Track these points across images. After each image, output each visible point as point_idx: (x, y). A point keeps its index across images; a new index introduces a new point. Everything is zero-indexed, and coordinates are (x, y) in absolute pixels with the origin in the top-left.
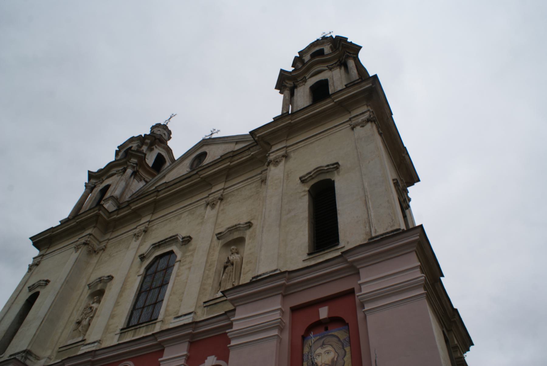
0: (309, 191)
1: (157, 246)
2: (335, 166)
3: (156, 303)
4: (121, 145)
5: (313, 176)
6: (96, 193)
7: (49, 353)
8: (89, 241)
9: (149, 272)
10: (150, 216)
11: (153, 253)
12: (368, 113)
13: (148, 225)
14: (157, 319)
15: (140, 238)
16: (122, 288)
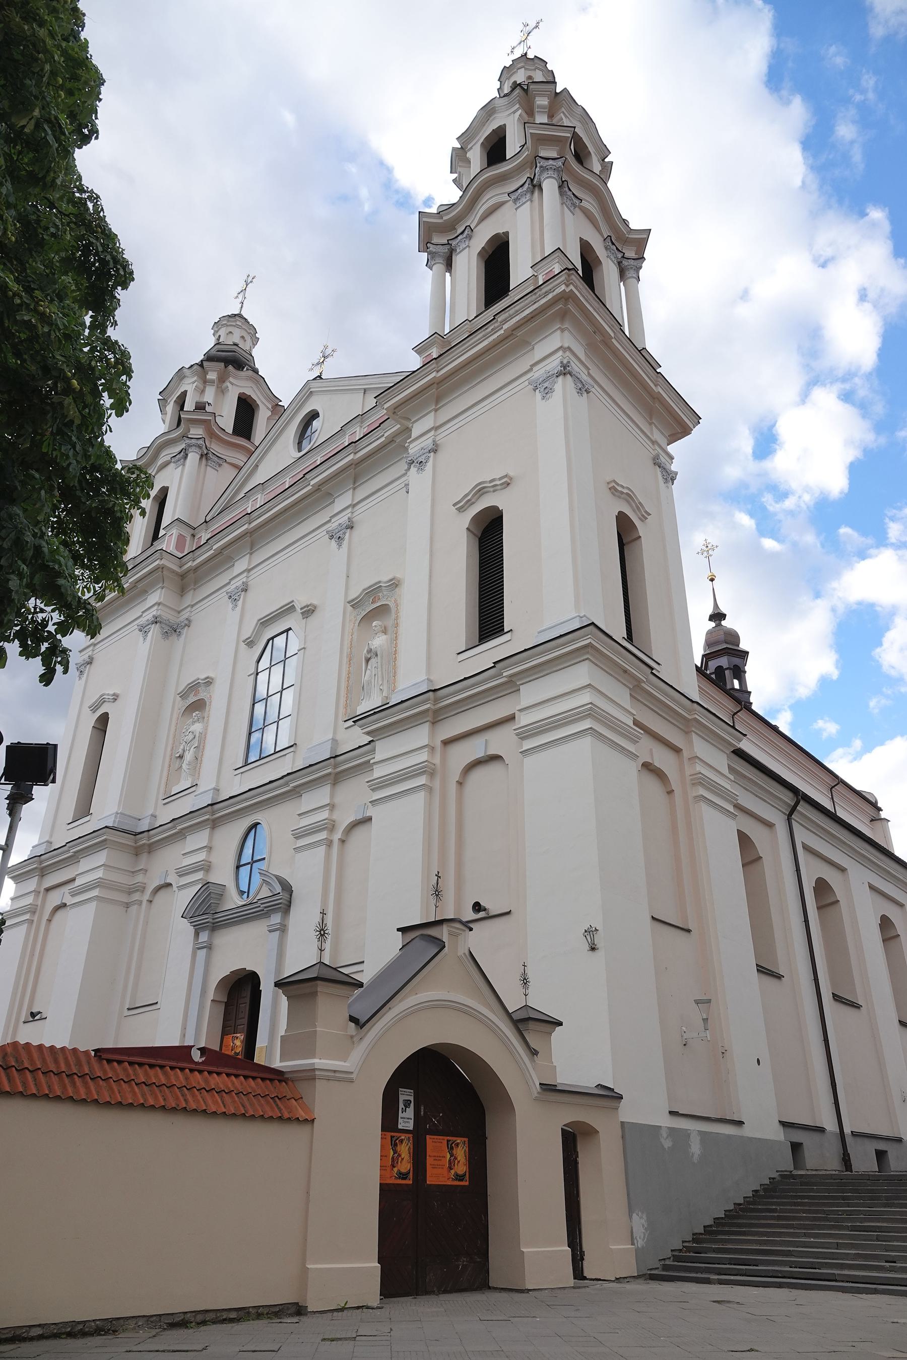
1: (265, 622)
12: (560, 353)
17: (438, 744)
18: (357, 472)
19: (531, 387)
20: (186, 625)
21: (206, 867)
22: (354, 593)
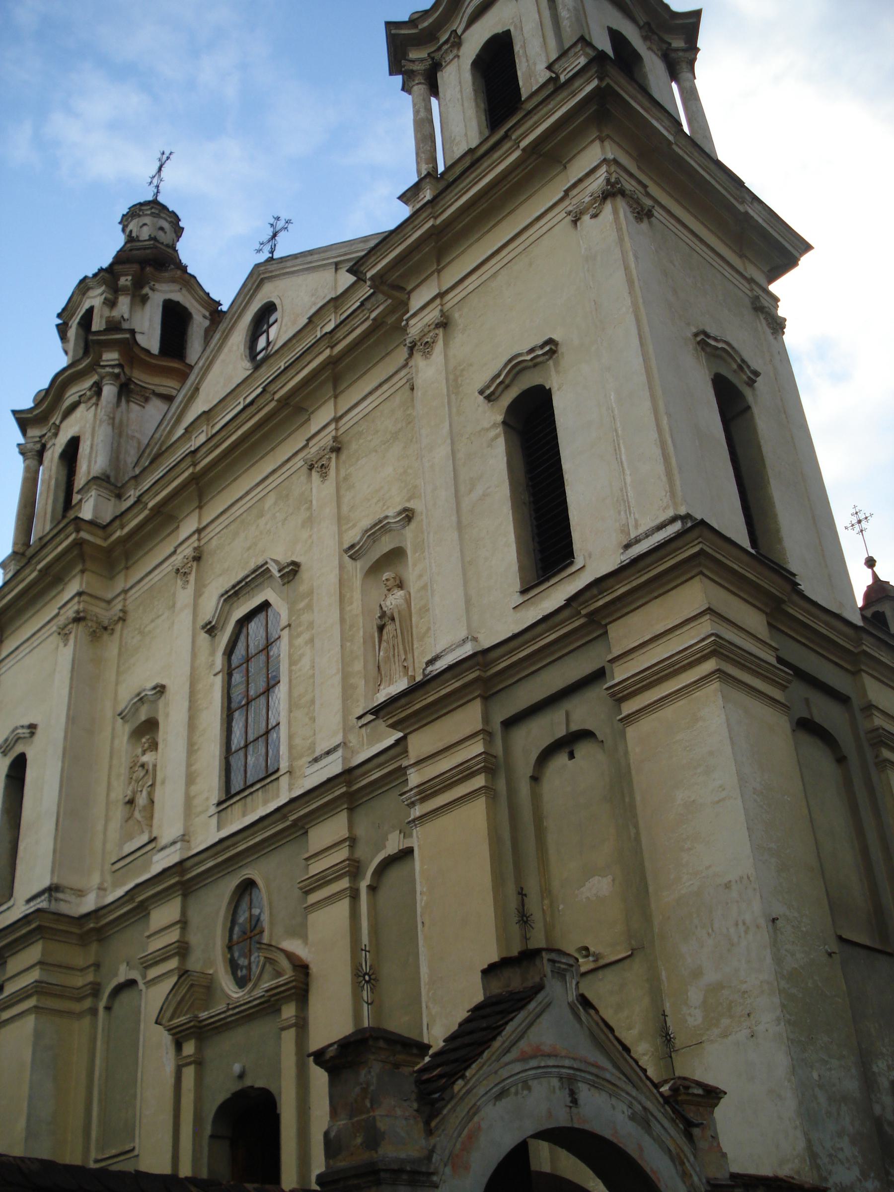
0: (504, 423)
1: (234, 594)
2: (547, 348)
3: (267, 732)
4: (64, 310)
5: (507, 382)
6: (54, 468)
7: (95, 880)
8: (84, 611)
9: (236, 659)
10: (195, 516)
11: (229, 614)
12: (604, 168)
13: (199, 540)
14: (278, 770)
15: (192, 578)
16: (190, 708)
17: (497, 727)
18: (335, 374)
19: (570, 218)
20: (120, 619)
21: (182, 950)
22: (353, 535)
